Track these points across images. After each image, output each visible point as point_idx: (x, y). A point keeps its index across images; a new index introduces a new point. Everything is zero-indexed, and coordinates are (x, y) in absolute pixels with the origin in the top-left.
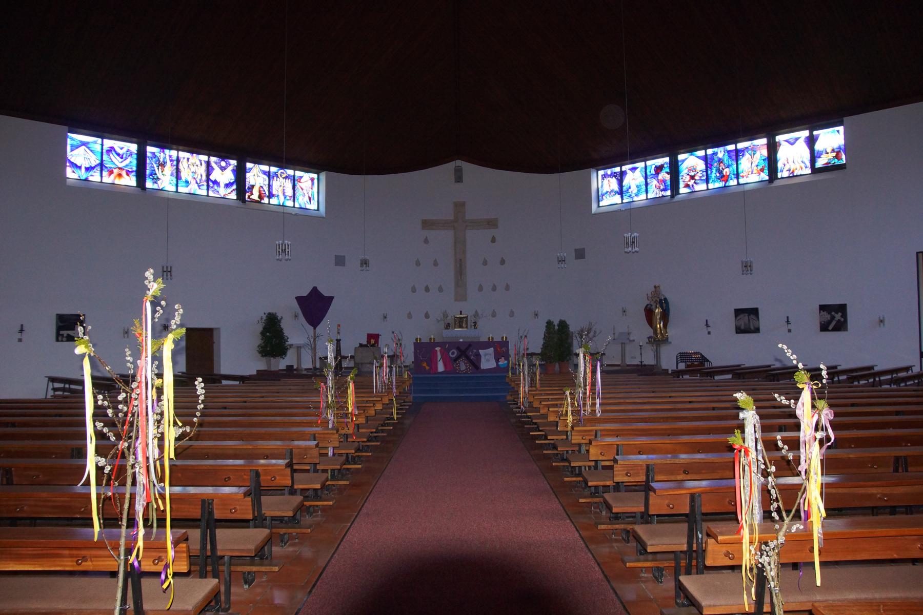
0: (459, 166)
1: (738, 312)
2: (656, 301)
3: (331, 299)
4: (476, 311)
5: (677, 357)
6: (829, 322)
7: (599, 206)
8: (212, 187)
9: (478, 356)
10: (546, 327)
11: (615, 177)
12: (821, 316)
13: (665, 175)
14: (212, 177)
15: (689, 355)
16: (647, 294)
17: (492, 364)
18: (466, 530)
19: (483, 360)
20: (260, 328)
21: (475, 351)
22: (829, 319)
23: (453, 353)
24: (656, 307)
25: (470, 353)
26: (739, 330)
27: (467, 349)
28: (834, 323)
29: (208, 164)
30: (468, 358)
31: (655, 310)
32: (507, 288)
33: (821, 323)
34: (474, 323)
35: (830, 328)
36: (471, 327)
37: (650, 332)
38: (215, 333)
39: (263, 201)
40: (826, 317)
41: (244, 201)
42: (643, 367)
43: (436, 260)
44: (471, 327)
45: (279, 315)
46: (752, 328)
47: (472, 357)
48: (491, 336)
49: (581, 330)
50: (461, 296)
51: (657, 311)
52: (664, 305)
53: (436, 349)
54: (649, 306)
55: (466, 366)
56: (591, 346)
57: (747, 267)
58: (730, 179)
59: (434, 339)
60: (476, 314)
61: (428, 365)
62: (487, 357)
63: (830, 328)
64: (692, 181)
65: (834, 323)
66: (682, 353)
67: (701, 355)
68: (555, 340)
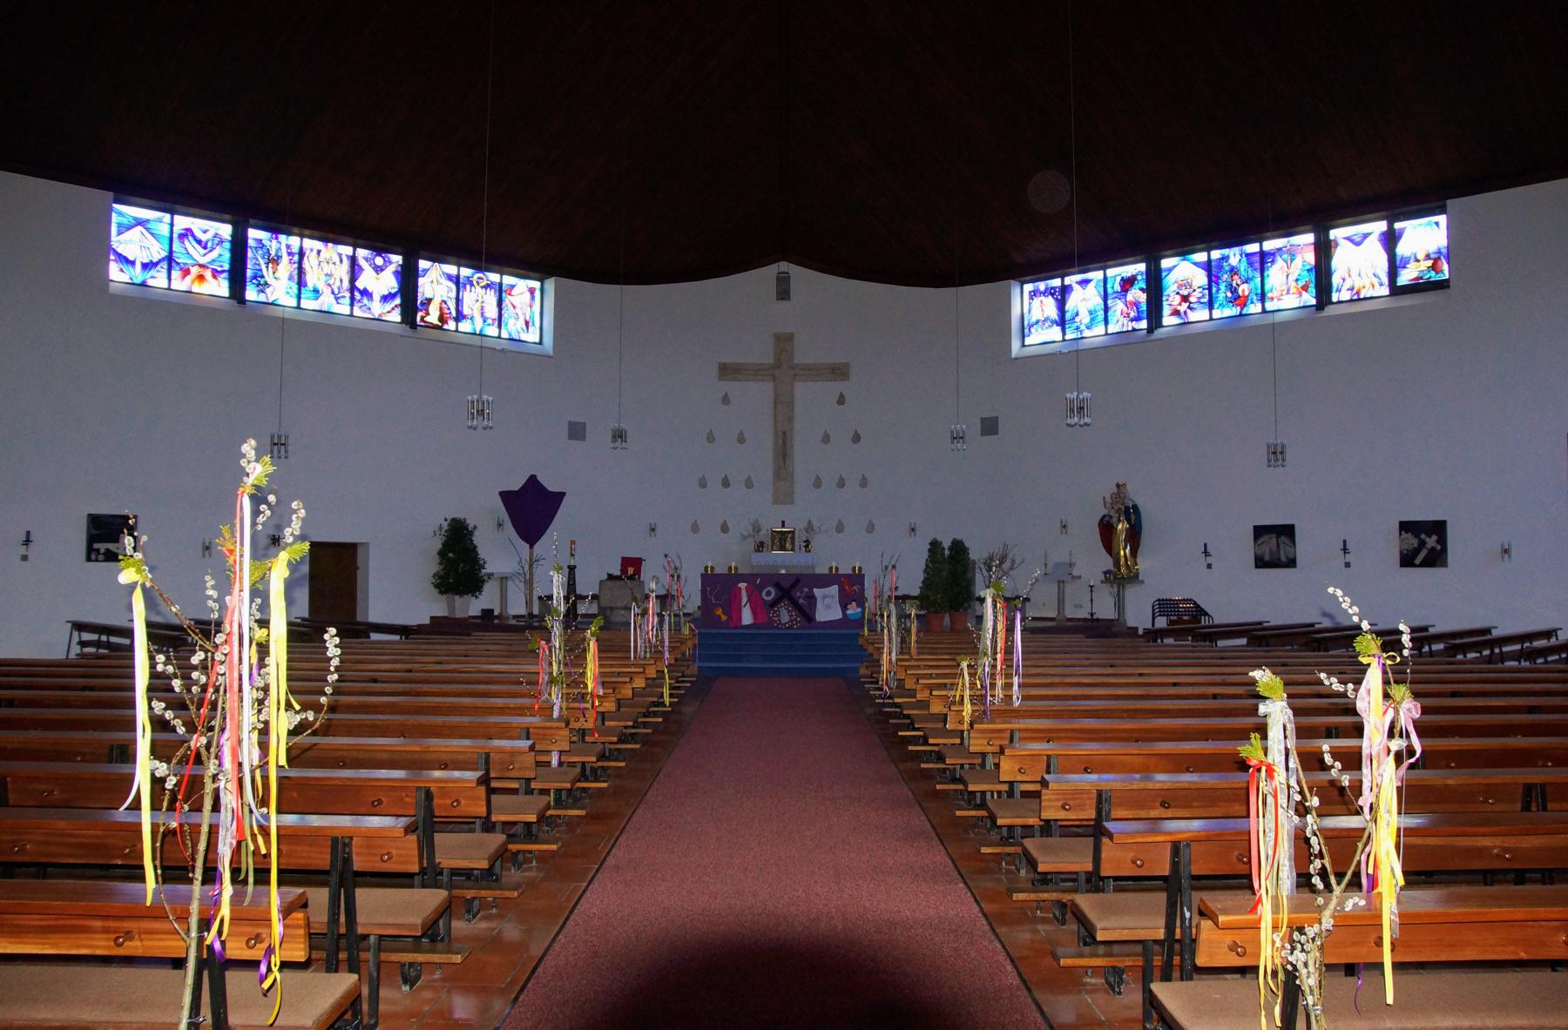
1: (1260, 531)
2: (1118, 511)
3: (561, 495)
6: (1416, 551)
8: (359, 301)
9: (812, 599)
10: (930, 550)
11: (1052, 295)
12: (1401, 541)
13: (1137, 294)
14: (360, 284)
16: (1104, 498)
18: (786, 897)
19: (819, 605)
22: (1416, 545)
23: (768, 594)
24: (1119, 521)
25: (798, 594)
26: (1261, 563)
27: (793, 586)
28: (1424, 553)
29: (353, 260)
30: (794, 603)
33: (1401, 553)
34: (804, 542)
35: (1417, 561)
36: (800, 549)
37: (1108, 563)
39: (446, 327)
40: (1411, 542)
41: (414, 325)
43: (741, 433)
44: (800, 549)
46: (1283, 558)
47: (801, 601)
50: (783, 495)
51: (1120, 527)
53: (740, 585)
54: (1107, 519)
57: (1276, 454)
58: (1249, 302)
60: (810, 528)
62: (827, 601)
63: (1417, 561)
64: (1185, 305)
65: (1424, 553)
66: (1163, 600)
68: (945, 574)
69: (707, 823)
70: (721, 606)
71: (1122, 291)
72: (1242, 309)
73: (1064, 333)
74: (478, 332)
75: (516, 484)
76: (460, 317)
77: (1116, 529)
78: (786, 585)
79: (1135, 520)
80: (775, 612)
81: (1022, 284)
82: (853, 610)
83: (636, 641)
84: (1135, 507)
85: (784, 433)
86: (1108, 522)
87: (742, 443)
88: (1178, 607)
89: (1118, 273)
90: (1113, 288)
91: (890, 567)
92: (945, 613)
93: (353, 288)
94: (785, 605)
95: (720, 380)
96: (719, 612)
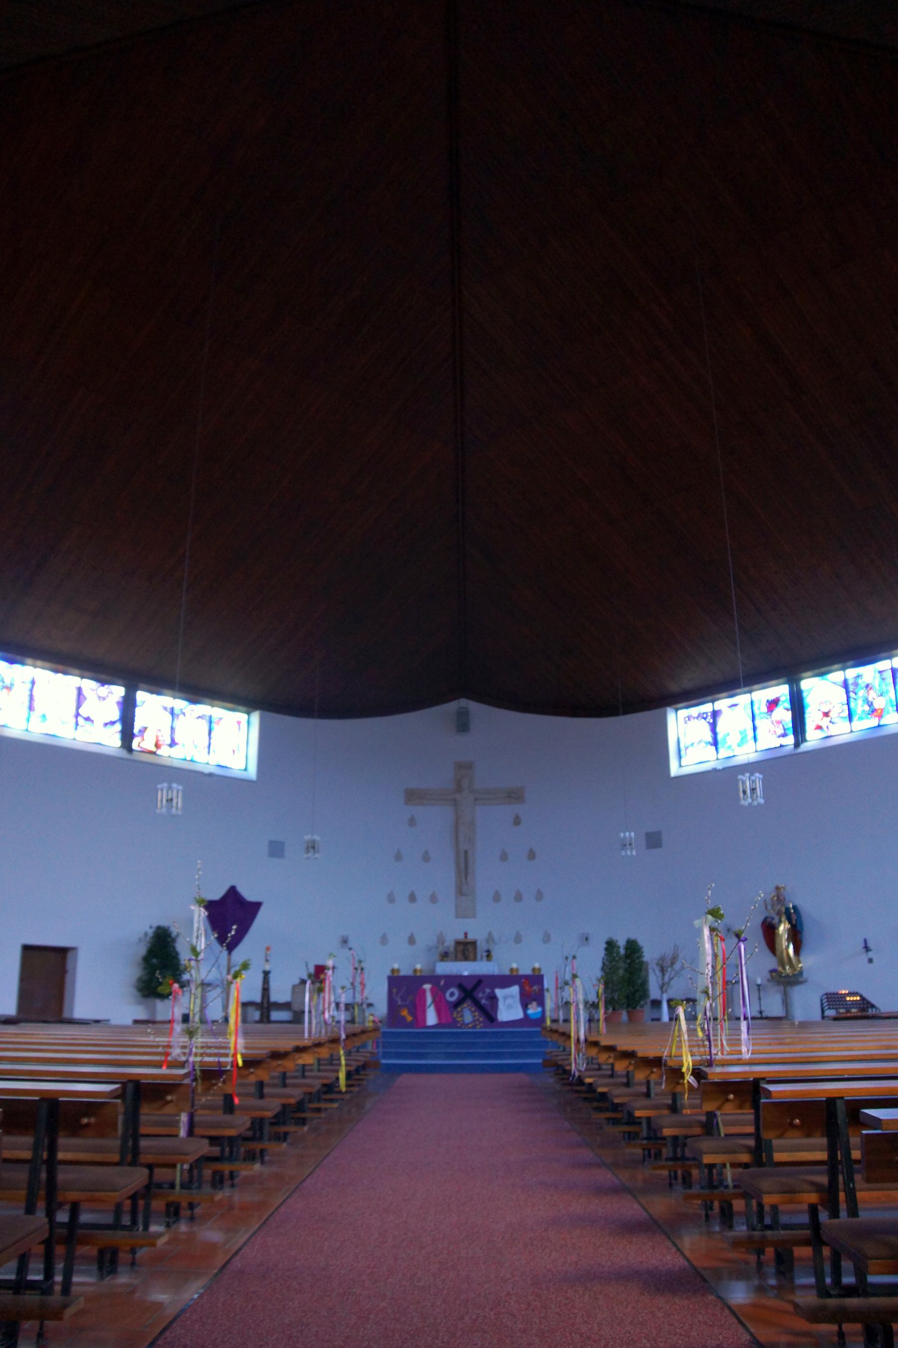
0: (463, 708)
2: (779, 913)
3: (257, 906)
4: (490, 934)
7: (680, 766)
9: (493, 999)
10: (606, 949)
11: (705, 719)
13: (784, 714)
15: (841, 997)
18: (467, 1318)
19: (501, 1005)
20: (143, 951)
21: (488, 991)
23: (452, 994)
25: (480, 995)
27: (475, 987)
29: (80, 690)
30: (477, 1003)
37: (771, 962)
38: (70, 955)
41: (130, 750)
45: (174, 931)
47: (483, 1001)
49: (661, 959)
52: (794, 917)
55: (474, 1016)
60: (490, 938)
61: (410, 1013)
62: (509, 1001)
64: (827, 719)
66: (830, 994)
67: (861, 996)
68: (621, 972)
69: (371, 1215)
71: (768, 712)
72: (879, 720)
75: (216, 894)
78: (469, 986)
79: (796, 920)
80: (458, 1012)
81: (677, 710)
83: (310, 1023)
85: (466, 852)
88: (846, 1004)
89: (762, 695)
90: (759, 709)
91: (570, 958)
92: (623, 1010)
93: (77, 715)
94: (468, 1006)
96: (405, 1013)
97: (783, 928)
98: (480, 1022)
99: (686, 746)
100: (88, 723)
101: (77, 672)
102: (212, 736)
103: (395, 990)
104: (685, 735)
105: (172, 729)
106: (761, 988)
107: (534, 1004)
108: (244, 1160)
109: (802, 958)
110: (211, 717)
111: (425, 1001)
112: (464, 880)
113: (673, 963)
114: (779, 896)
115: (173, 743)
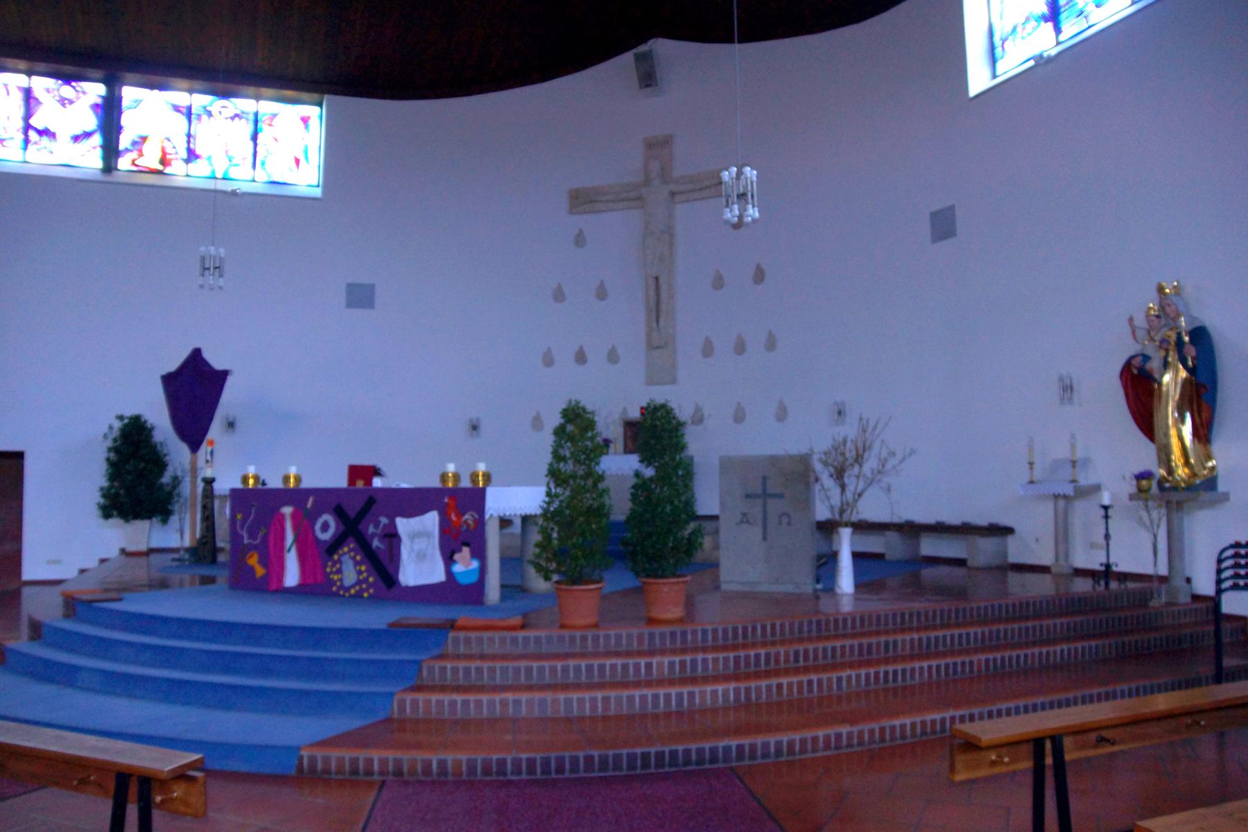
3: (224, 375)
5: (1220, 561)
8: (36, 143)
9: (392, 537)
14: (37, 121)
16: (1131, 320)
17: (435, 573)
23: (325, 527)
24: (1166, 365)
29: (28, 94)
30: (364, 545)
31: (1162, 376)
32: (771, 344)
39: (168, 170)
42: (1114, 585)
47: (376, 543)
48: (293, 471)
50: (663, 374)
51: (1167, 378)
54: (1136, 362)
55: (360, 572)
56: (570, 515)
59: (298, 479)
70: (256, 548)
73: (1058, 30)
74: (219, 176)
76: (192, 155)
77: (1160, 384)
78: (352, 511)
80: (335, 563)
82: (465, 566)
84: (1200, 335)
86: (1141, 369)
87: (602, 299)
93: (28, 127)
94: (351, 550)
95: (571, 213)
96: (253, 560)
97: (1171, 380)
98: (370, 586)
99: (1003, 37)
100: (45, 138)
101: (22, 64)
102: (258, 141)
103: (239, 517)
104: (1001, 18)
105: (189, 136)
106: (1110, 512)
107: (466, 551)
108: (130, 775)
109: (1216, 447)
110: (256, 114)
111: (282, 538)
112: (654, 324)
113: (859, 459)
114: (1166, 310)
115: (192, 155)
